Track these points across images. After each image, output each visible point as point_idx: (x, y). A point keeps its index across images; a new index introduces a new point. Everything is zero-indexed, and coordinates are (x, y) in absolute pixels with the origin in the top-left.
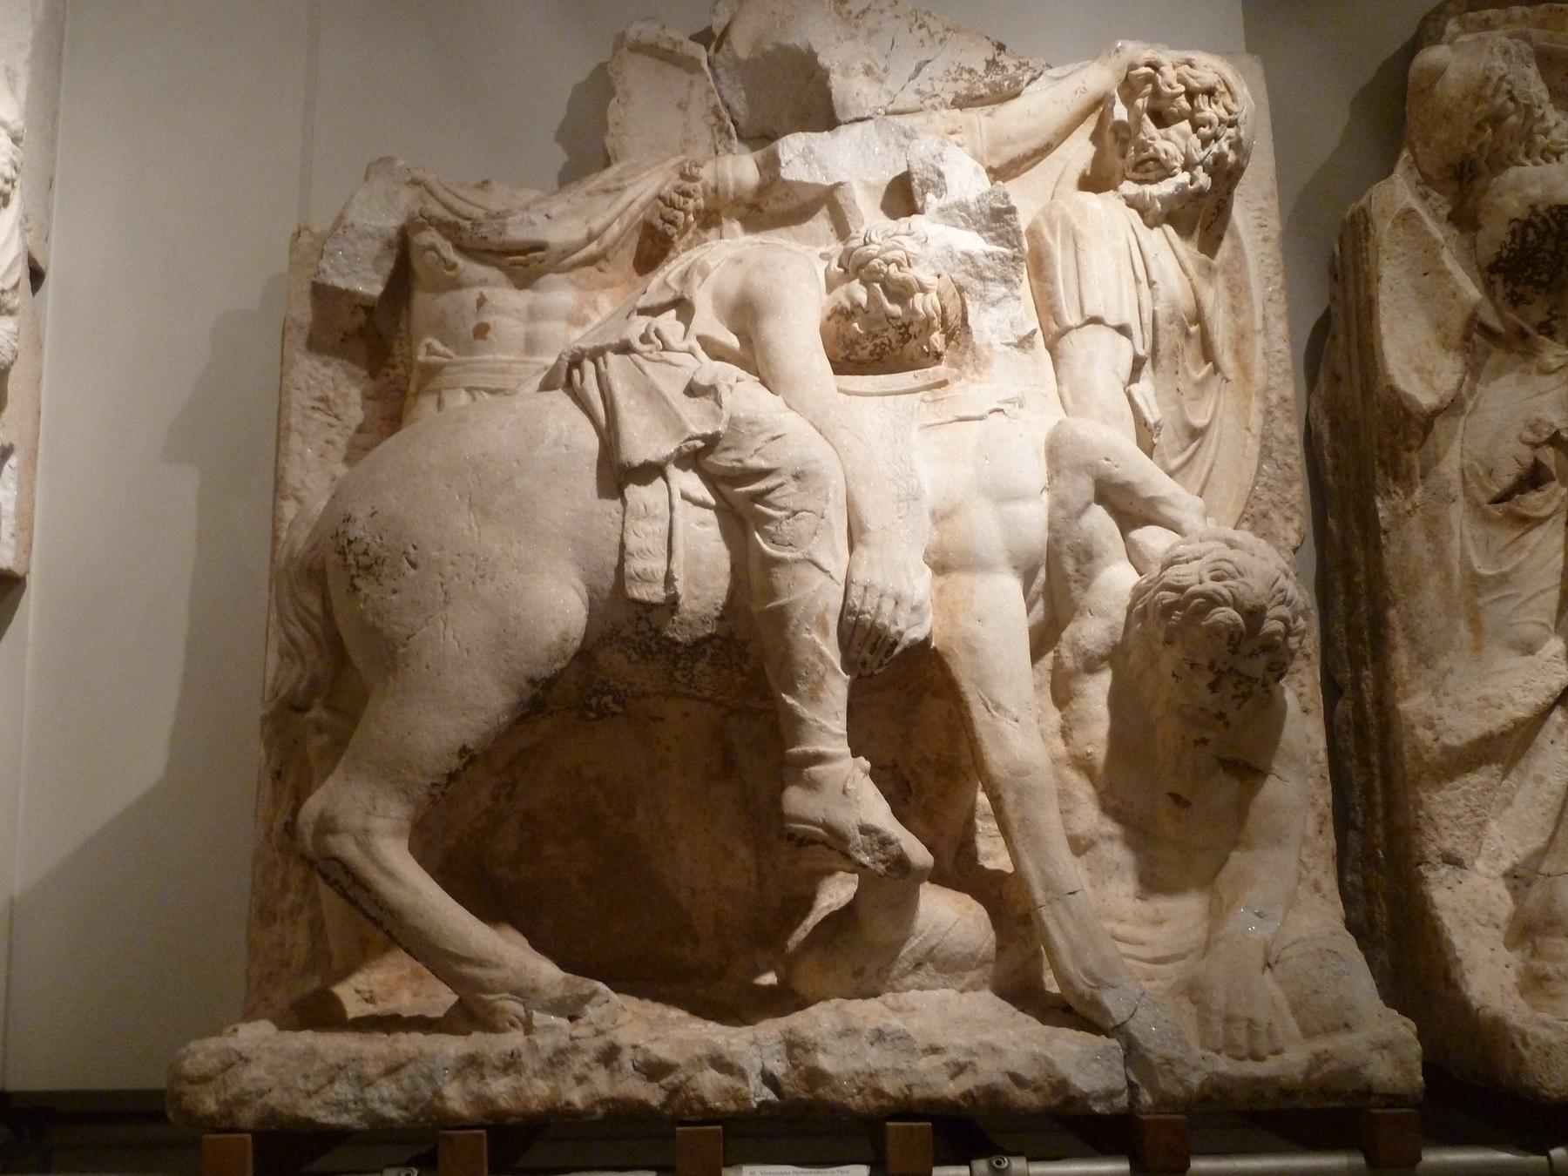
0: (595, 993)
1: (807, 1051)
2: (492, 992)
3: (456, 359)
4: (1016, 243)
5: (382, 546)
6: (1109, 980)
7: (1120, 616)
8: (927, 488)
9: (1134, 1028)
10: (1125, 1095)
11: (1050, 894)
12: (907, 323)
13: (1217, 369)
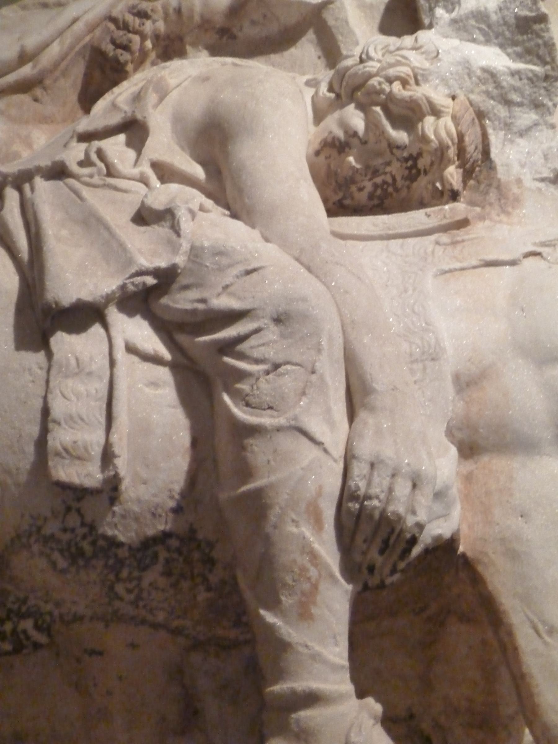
4: (548, 59)
8: (448, 344)
12: (415, 154)
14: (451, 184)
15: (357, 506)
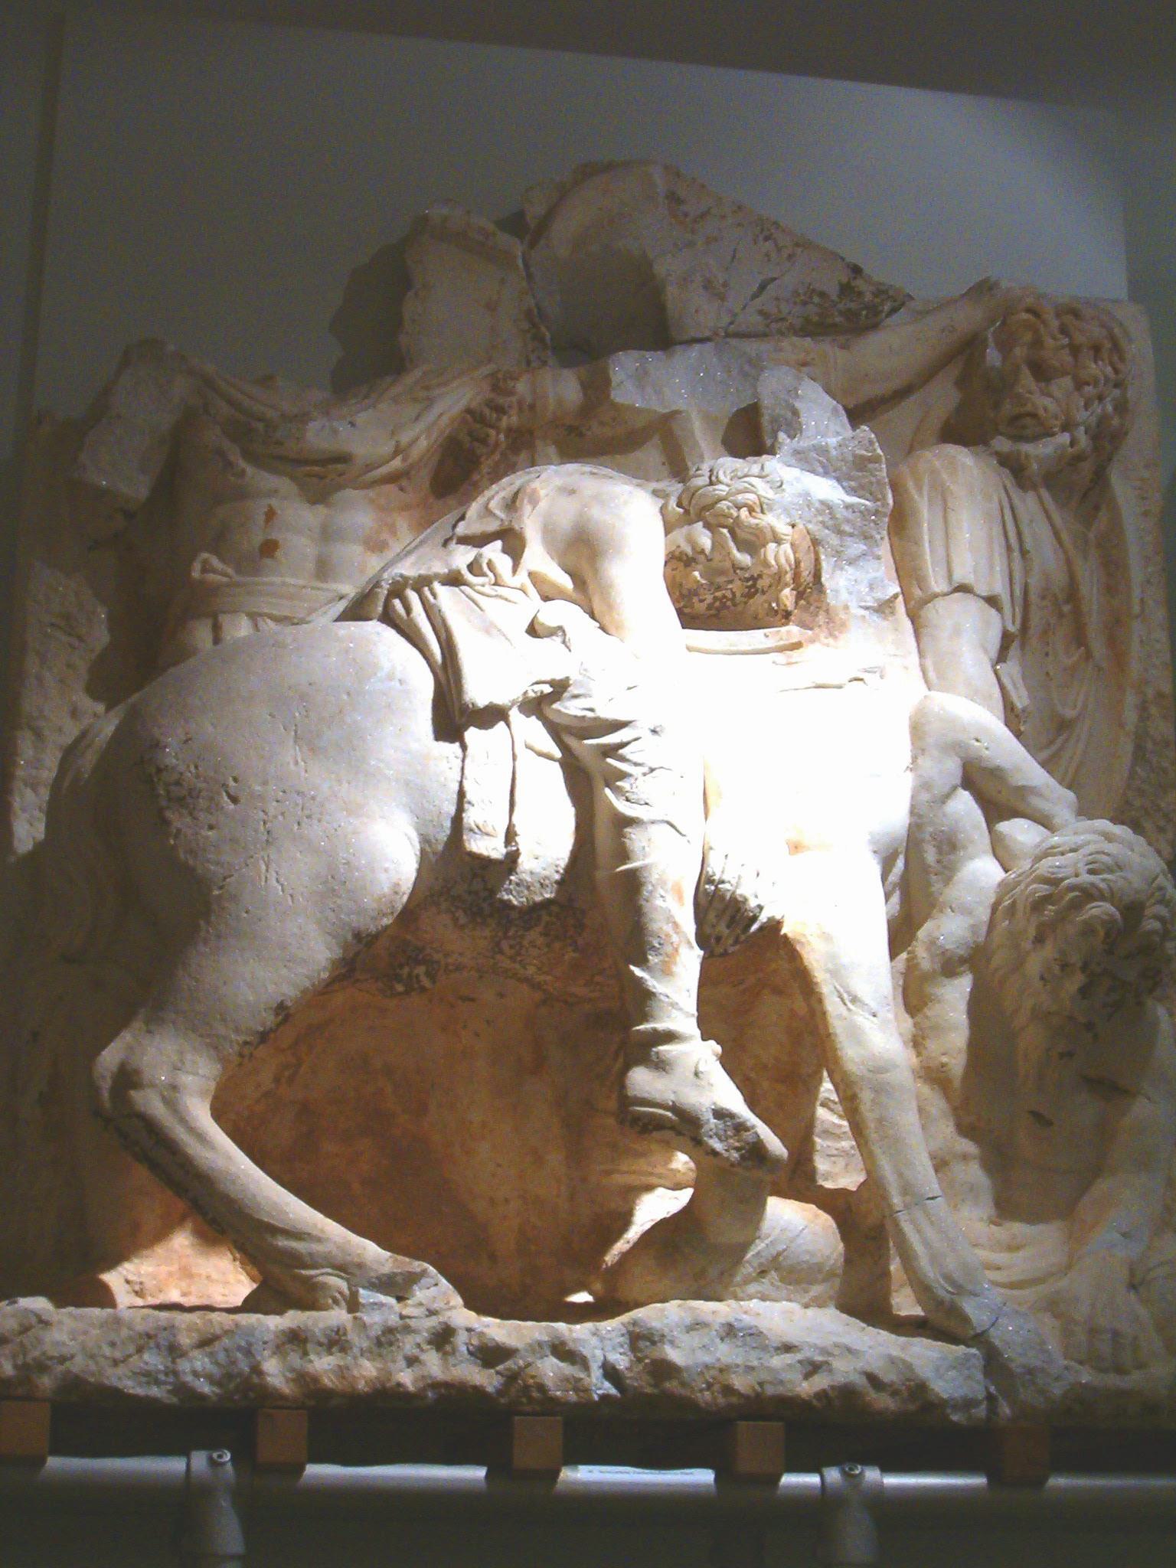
0: (424, 1273)
1: (654, 1343)
2: (314, 1267)
3: (237, 578)
4: (880, 496)
5: (198, 777)
6: (970, 1287)
7: (983, 914)
9: (996, 1337)
10: (984, 1406)
11: (908, 1198)
13: (1088, 656)
14: (785, 606)
15: (713, 888)
